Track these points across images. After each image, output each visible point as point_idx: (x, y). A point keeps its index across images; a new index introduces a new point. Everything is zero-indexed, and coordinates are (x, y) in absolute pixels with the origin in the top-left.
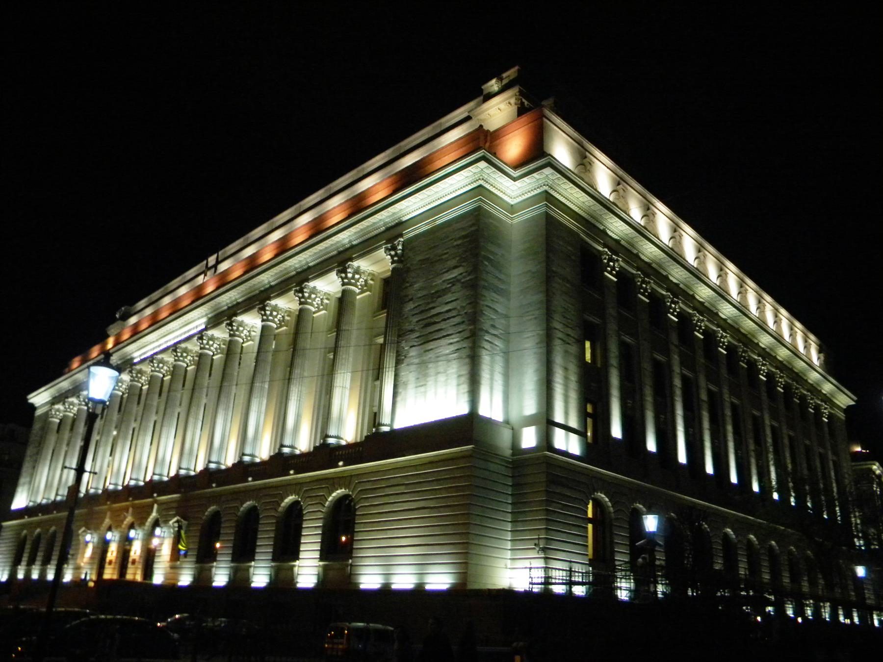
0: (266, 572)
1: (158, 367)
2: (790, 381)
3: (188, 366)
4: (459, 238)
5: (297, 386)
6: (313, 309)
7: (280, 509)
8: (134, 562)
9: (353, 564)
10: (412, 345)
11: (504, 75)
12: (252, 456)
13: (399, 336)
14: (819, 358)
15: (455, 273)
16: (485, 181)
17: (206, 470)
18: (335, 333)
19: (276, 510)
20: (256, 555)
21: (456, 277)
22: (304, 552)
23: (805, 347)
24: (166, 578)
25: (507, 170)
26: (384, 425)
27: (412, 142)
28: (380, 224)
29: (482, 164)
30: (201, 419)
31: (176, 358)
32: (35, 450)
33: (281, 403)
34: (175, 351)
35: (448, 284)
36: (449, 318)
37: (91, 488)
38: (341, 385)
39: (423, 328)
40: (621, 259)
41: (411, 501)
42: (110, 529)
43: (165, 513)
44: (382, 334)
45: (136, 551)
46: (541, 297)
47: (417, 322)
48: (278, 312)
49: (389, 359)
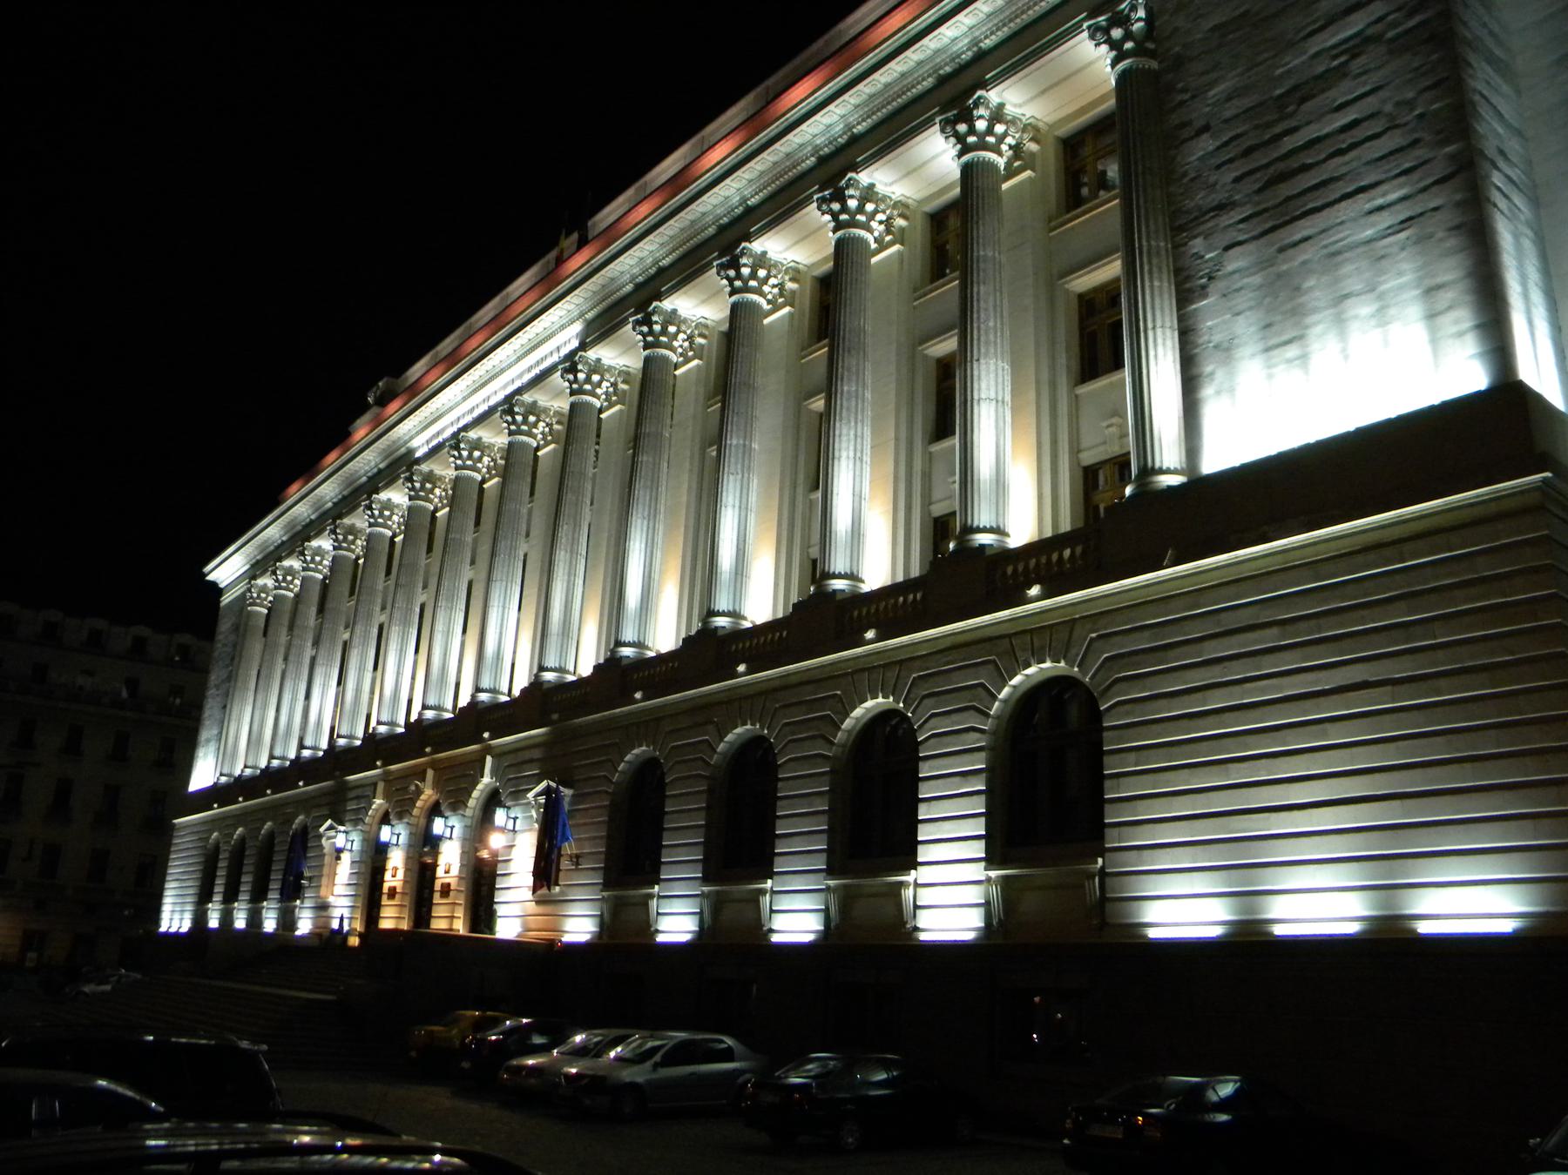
1: (470, 457)
6: (674, 358)
7: (840, 737)
8: (446, 890)
10: (1226, 243)
12: (561, 670)
13: (1177, 230)
17: (536, 686)
24: (527, 929)
26: (1162, 471)
30: (584, 553)
31: (513, 427)
32: (224, 674)
34: (510, 412)
35: (1335, 57)
42: (385, 820)
44: (1117, 251)
47: (1237, 180)
48: (538, 417)
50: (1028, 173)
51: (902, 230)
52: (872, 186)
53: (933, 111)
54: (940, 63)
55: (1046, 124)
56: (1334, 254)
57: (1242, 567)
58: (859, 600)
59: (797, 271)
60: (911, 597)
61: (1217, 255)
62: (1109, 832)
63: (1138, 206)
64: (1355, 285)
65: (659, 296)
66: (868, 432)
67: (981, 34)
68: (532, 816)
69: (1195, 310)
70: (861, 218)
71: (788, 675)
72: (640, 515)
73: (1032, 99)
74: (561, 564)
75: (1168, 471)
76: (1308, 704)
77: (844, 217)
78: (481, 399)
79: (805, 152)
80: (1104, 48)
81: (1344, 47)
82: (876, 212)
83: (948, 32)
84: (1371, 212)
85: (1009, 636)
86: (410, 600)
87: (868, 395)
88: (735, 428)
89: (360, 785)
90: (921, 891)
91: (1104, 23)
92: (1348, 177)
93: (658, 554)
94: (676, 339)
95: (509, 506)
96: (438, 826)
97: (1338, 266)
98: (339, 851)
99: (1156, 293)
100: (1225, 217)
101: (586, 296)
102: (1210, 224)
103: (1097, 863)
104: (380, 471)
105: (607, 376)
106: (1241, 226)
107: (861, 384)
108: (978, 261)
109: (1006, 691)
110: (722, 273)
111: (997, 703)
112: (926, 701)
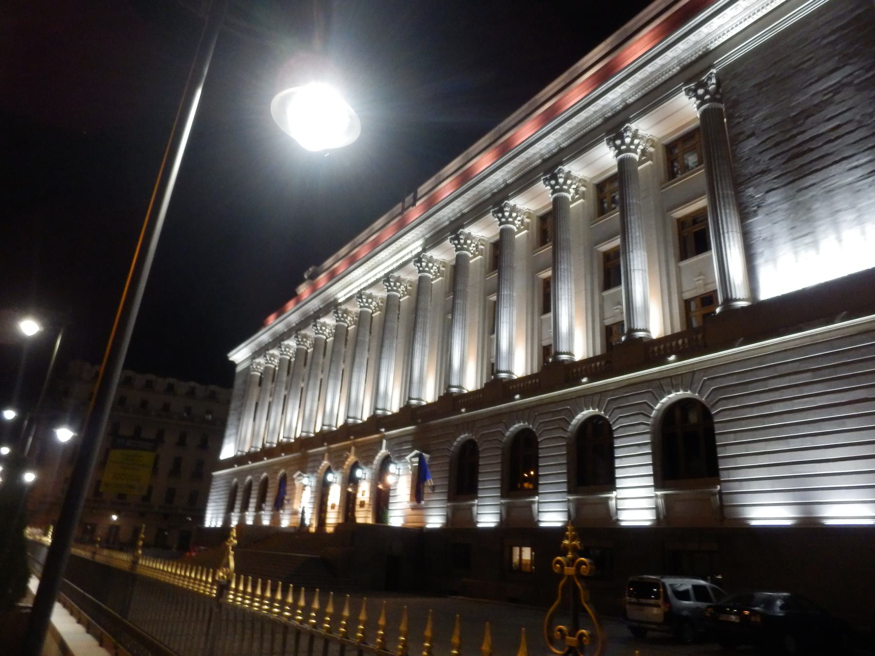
0: (562, 507)
1: (367, 302)
3: (327, 338)
4: (831, 34)
6: (431, 277)
7: (570, 428)
8: (362, 504)
10: (767, 189)
18: (452, 296)
20: (479, 492)
21: (839, 82)
24: (406, 522)
26: (736, 300)
31: (389, 288)
33: (408, 364)
34: (388, 281)
35: (825, 95)
37: (267, 442)
39: (784, 163)
43: (396, 449)
44: (703, 194)
45: (364, 493)
47: (772, 158)
49: (726, 218)
50: (649, 162)
51: (583, 192)
52: (570, 172)
53: (602, 135)
54: (605, 111)
55: (589, 178)
56: (830, 191)
57: (764, 350)
58: (512, 382)
59: (529, 213)
60: (534, 381)
61: (762, 195)
63: (716, 175)
64: (842, 205)
65: (463, 227)
66: (573, 286)
67: (627, 96)
68: (408, 468)
69: (751, 223)
70: (565, 187)
71: (542, 400)
72: (458, 327)
73: (652, 127)
74: (418, 351)
75: (739, 300)
76: (833, 409)
77: (557, 187)
78: (381, 273)
79: (536, 157)
80: (694, 99)
81: (831, 89)
82: (517, 216)
83: (610, 96)
84: (850, 169)
85: (659, 379)
86: (337, 368)
87: (572, 270)
88: (505, 286)
89: (315, 455)
90: (619, 501)
91: (693, 87)
92: (836, 153)
93: (467, 346)
94: (400, 288)
95: (389, 324)
96: (359, 473)
97: (832, 197)
98: (305, 486)
99: (728, 215)
100: (766, 177)
101: (425, 227)
102: (757, 181)
103: (716, 488)
104: (320, 309)
105: (435, 264)
106: (775, 181)
107: (569, 264)
108: (629, 205)
109: (658, 406)
110: (452, 242)
112: (616, 411)
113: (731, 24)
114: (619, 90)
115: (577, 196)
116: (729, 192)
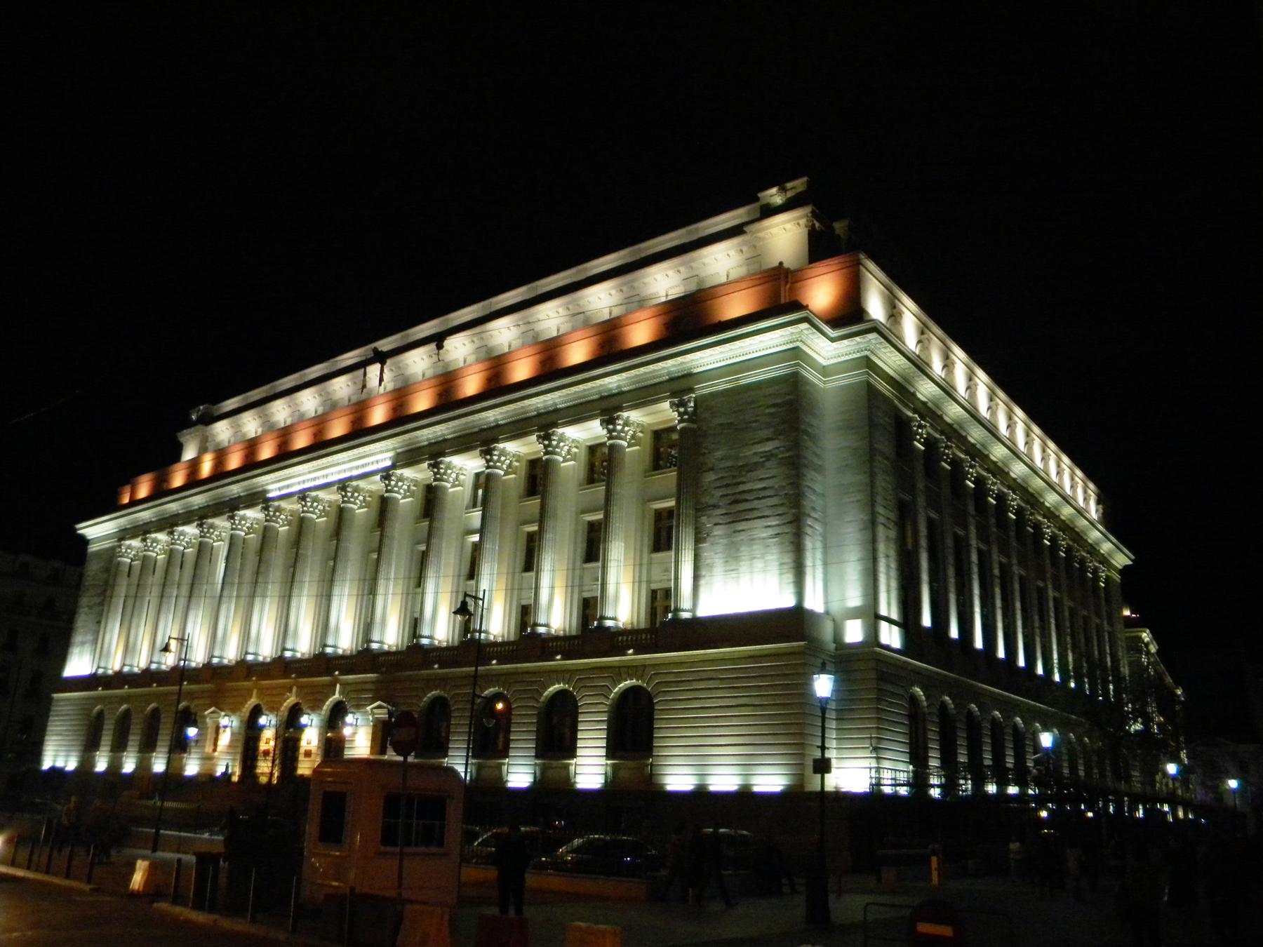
2: (1023, 505)
5: (550, 553)
7: (542, 699)
9: (654, 763)
10: (714, 523)
11: (789, 185)
13: (697, 510)
14: (1097, 511)
15: (769, 447)
16: (803, 342)
19: (537, 701)
20: (450, 750)
21: (770, 451)
22: (581, 749)
23: (1043, 459)
25: (826, 330)
27: (661, 244)
28: (663, 372)
29: (805, 325)
35: (761, 457)
36: (764, 498)
38: (616, 558)
39: (730, 504)
40: (928, 425)
41: (728, 697)
46: (862, 478)
47: (722, 496)
50: (513, 476)
62: (654, 749)
68: (369, 719)
69: (703, 547)
81: (765, 454)
106: (722, 517)
109: (616, 690)
111: (613, 694)
112: (582, 689)
113: (769, 343)
114: (615, 378)
115: (568, 457)
116: (691, 512)
